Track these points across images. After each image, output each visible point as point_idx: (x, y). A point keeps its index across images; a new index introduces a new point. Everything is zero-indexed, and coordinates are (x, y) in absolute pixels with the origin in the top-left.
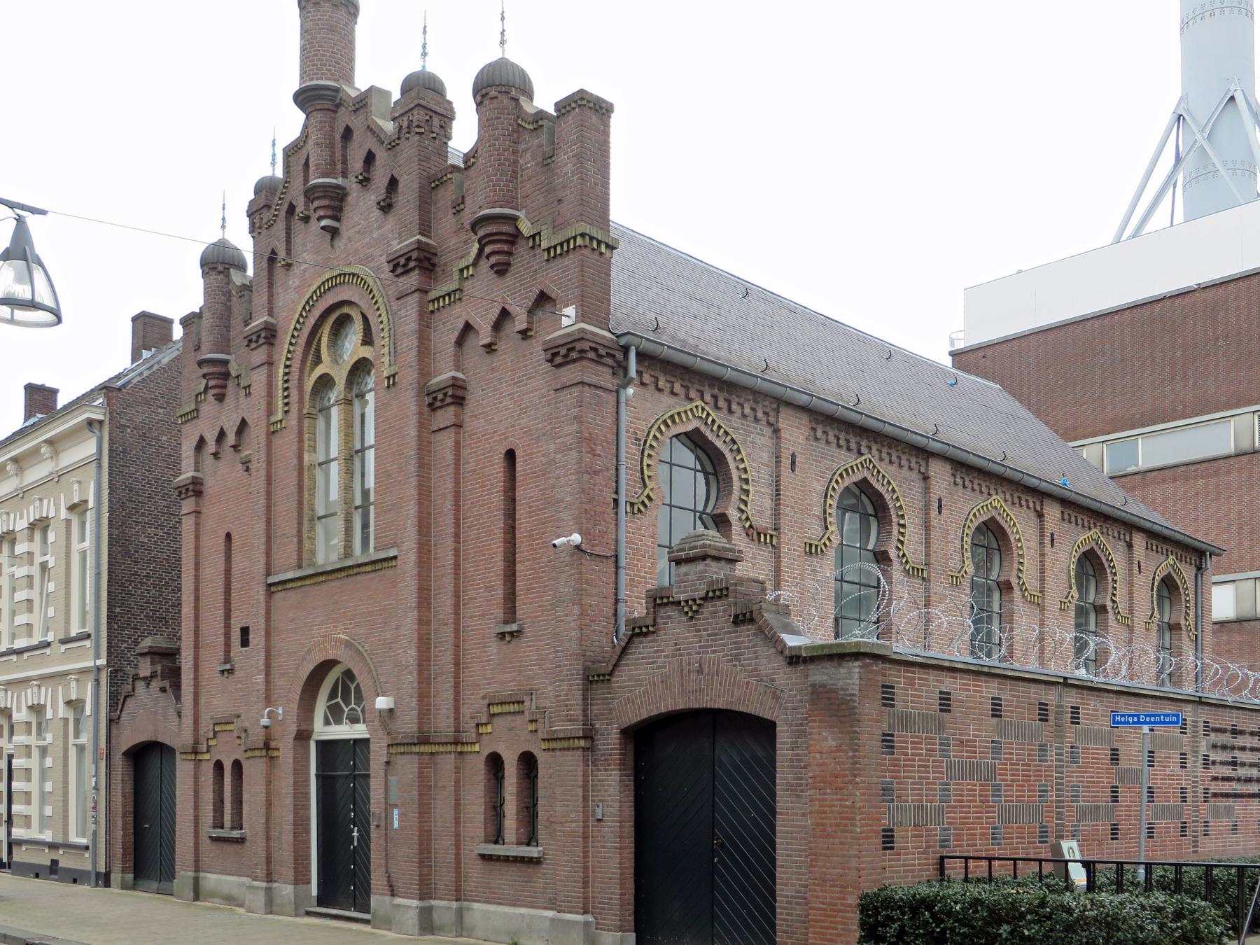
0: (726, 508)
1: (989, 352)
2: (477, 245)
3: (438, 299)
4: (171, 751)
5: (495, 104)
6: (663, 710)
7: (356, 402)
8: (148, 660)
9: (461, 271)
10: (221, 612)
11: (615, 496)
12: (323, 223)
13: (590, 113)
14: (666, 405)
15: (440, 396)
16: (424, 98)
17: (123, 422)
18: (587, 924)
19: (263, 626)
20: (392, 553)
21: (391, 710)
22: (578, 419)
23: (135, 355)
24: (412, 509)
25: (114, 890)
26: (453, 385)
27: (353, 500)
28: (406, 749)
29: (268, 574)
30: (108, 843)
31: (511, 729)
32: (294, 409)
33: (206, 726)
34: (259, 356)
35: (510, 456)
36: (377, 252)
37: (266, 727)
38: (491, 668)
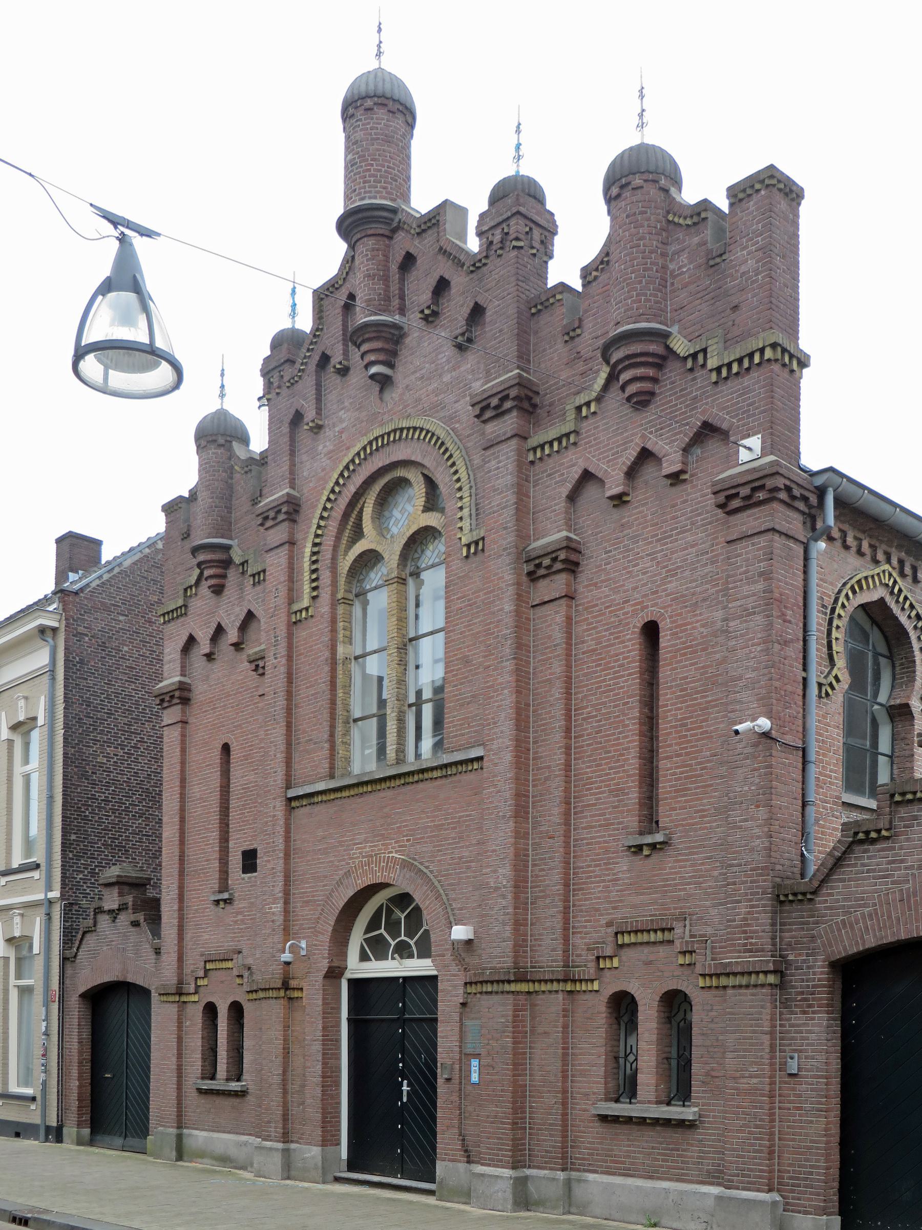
0: (909, 697)
3: (542, 446)
4: (145, 993)
5: (639, 195)
6: (903, 936)
7: (411, 582)
8: (115, 890)
9: (579, 409)
10: (215, 835)
11: (804, 674)
12: (374, 370)
13: (779, 196)
14: (853, 566)
15: (546, 562)
16: (520, 212)
17: (81, 629)
18: (774, 1203)
19: (282, 847)
21: (469, 942)
22: (766, 575)
24: (507, 699)
25: (68, 1146)
26: (567, 548)
27: (406, 696)
29: (288, 787)
30: (61, 1095)
31: (650, 963)
32: (325, 595)
33: (194, 963)
34: (279, 534)
35: (651, 631)
37: (288, 963)
38: (616, 890)
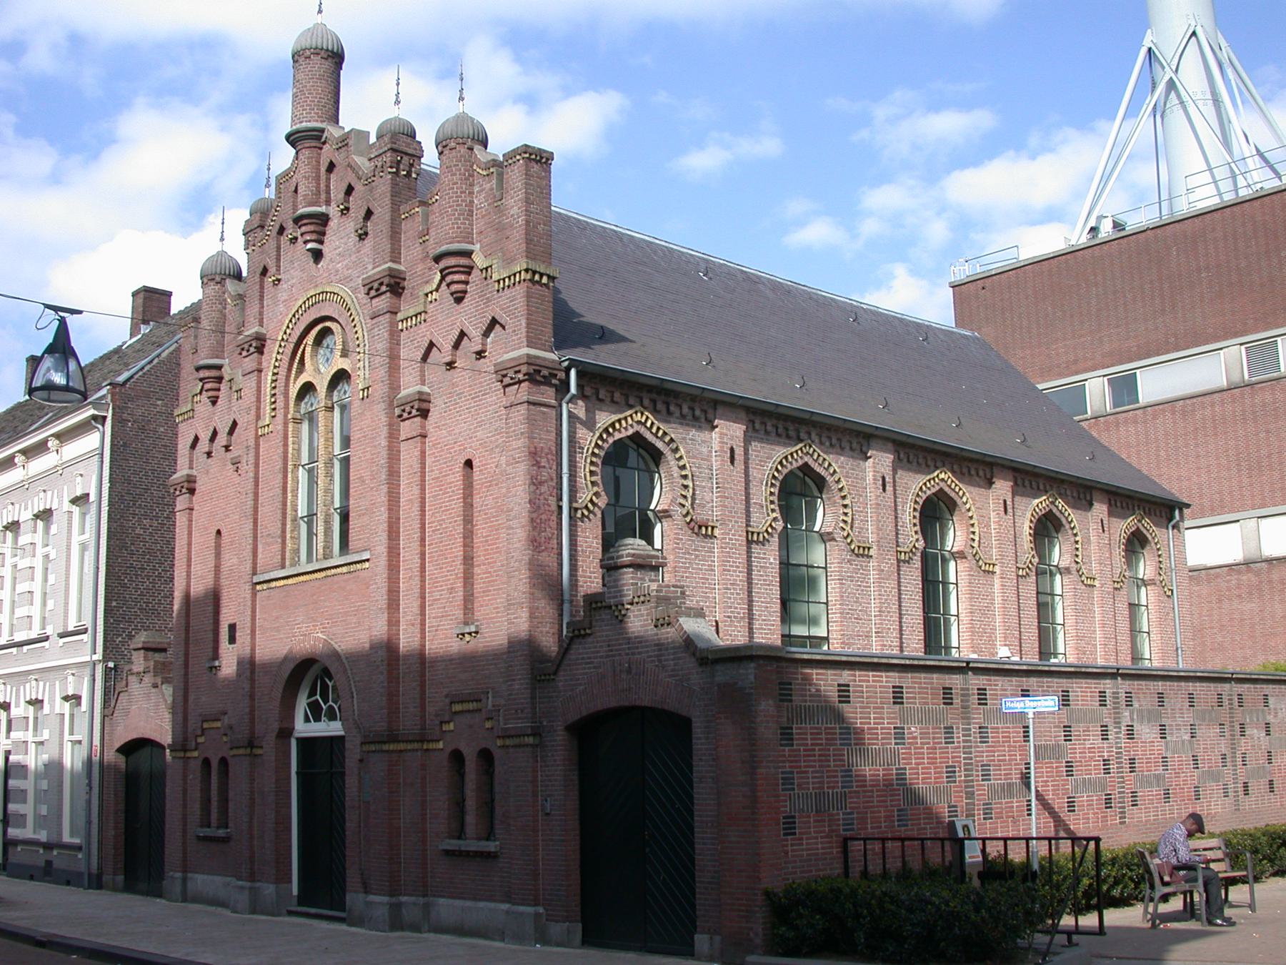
1: (988, 282)
2: (438, 277)
12: (310, 246)
15: (408, 409)
18: (537, 915)
19: (249, 625)
20: (366, 556)
23: (134, 330)
26: (420, 400)
28: (378, 747)
29: (254, 573)
31: (471, 726)
34: (250, 363)
36: (355, 273)
